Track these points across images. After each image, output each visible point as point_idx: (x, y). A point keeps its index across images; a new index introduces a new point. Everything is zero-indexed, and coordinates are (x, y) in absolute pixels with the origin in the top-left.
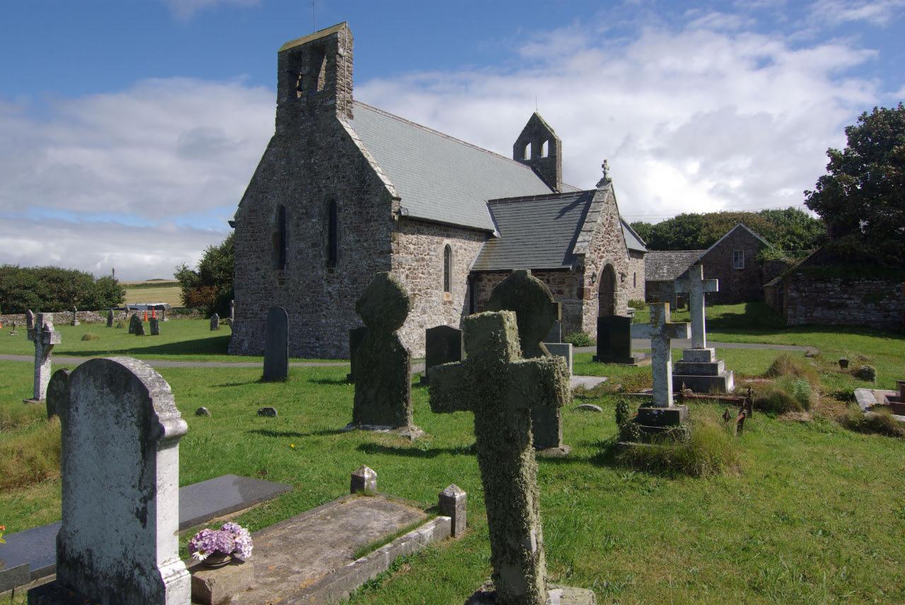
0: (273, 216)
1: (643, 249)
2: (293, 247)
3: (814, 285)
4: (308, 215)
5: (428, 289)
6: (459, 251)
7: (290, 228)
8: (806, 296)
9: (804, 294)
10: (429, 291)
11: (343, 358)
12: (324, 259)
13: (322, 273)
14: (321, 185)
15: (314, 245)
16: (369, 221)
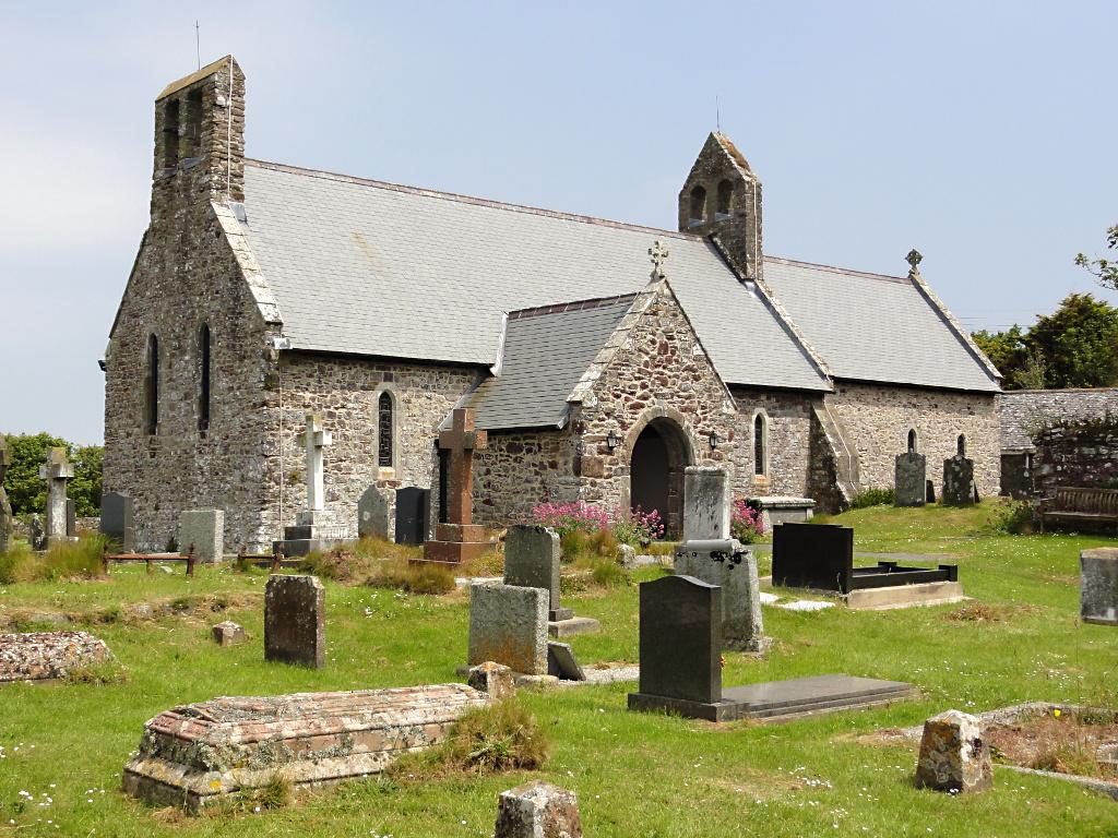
0: (145, 352)
1: (995, 387)
2: (167, 396)
3: (1076, 450)
4: (182, 350)
5: (341, 461)
6: (413, 400)
7: (162, 370)
8: (1063, 472)
9: (1059, 468)
10: (343, 464)
11: (627, 661)
12: (196, 417)
13: (194, 437)
14: (195, 305)
15: (187, 396)
16: (242, 358)
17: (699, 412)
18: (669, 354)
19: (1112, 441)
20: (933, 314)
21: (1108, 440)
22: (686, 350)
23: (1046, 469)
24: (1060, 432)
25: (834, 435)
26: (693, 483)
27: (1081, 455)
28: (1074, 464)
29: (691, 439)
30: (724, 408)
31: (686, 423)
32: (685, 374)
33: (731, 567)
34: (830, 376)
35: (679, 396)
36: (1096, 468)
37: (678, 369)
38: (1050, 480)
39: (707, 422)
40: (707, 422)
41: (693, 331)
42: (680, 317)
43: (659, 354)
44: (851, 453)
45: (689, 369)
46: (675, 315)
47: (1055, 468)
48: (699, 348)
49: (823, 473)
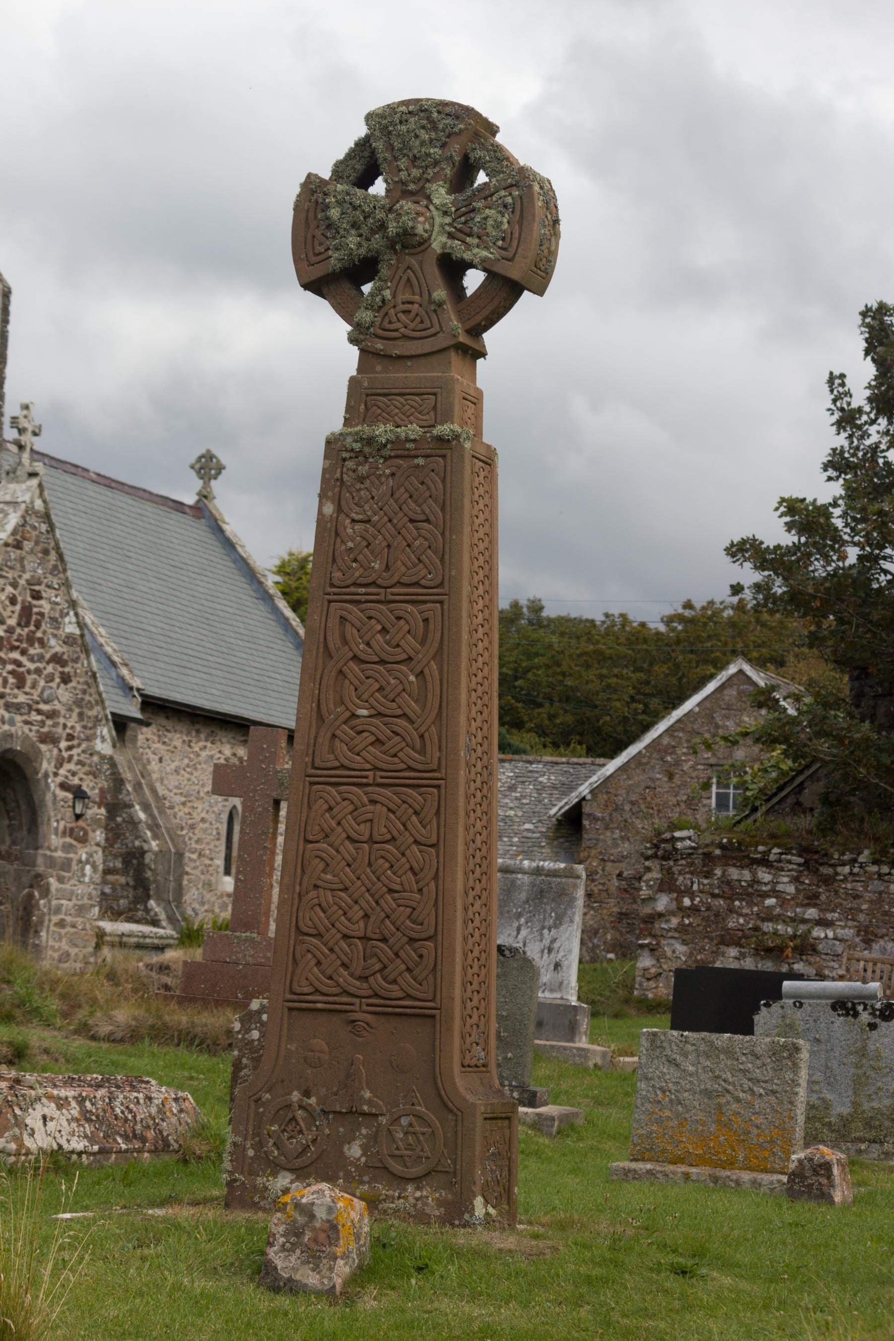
3: (718, 872)
8: (694, 909)
9: (687, 902)
17: (63, 744)
18: (32, 628)
19: (780, 861)
20: (241, 582)
21: (772, 857)
22: (56, 622)
23: (663, 902)
24: (690, 838)
25: (146, 807)
26: (510, 889)
27: (726, 882)
28: (714, 896)
29: (49, 797)
30: (98, 741)
31: (45, 765)
32: (50, 669)
33: (873, 1027)
34: (138, 690)
35: (39, 712)
36: (750, 904)
37: (41, 658)
38: (668, 921)
39: (72, 766)
40: (72, 766)
41: (67, 584)
42: (53, 556)
43: (19, 624)
44: (175, 846)
45: (57, 659)
46: (46, 552)
47: (679, 901)
48: (74, 620)
49: (122, 880)
